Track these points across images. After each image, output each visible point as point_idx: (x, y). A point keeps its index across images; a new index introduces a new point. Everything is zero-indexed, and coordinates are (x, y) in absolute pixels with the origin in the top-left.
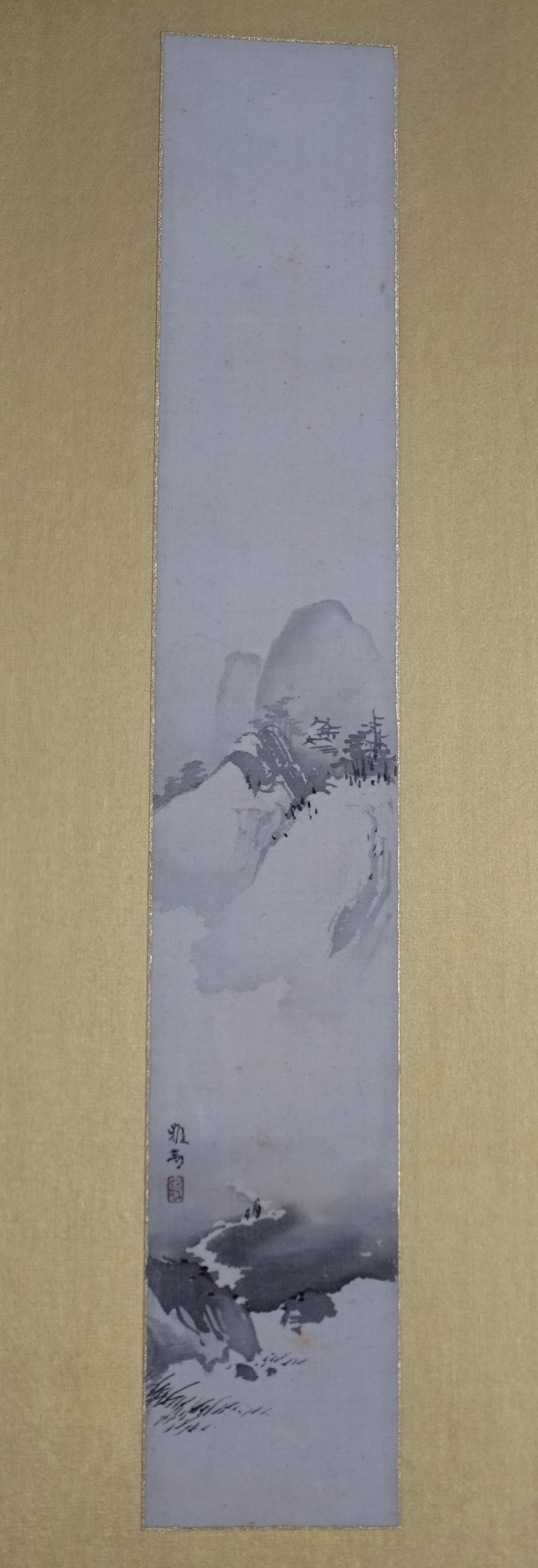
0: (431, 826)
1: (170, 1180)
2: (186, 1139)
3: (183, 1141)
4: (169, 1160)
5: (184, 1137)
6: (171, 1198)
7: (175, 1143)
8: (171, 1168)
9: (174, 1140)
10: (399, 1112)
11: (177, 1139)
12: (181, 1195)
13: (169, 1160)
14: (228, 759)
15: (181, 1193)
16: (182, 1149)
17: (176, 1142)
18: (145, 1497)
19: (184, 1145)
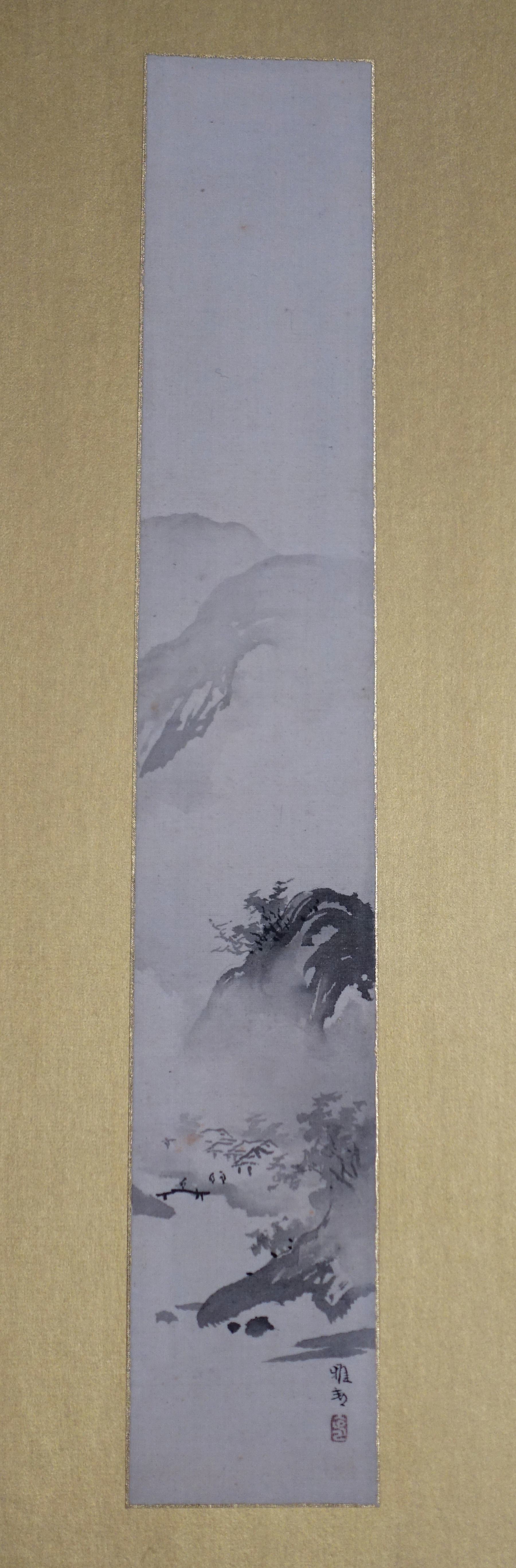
0: (5, 384)
1: (334, 1419)
2: (350, 1379)
3: (347, 1380)
4: (233, 1166)
5: (347, 1375)
6: (335, 1438)
7: (337, 1381)
8: (335, 1407)
9: (336, 1378)
10: (375, 745)
11: (340, 1376)
12: (345, 1434)
13: (233, 1166)
14: (368, 999)
15: (345, 1432)
16: (343, 1387)
17: (339, 1380)
18: (131, 1159)
19: (347, 1384)
